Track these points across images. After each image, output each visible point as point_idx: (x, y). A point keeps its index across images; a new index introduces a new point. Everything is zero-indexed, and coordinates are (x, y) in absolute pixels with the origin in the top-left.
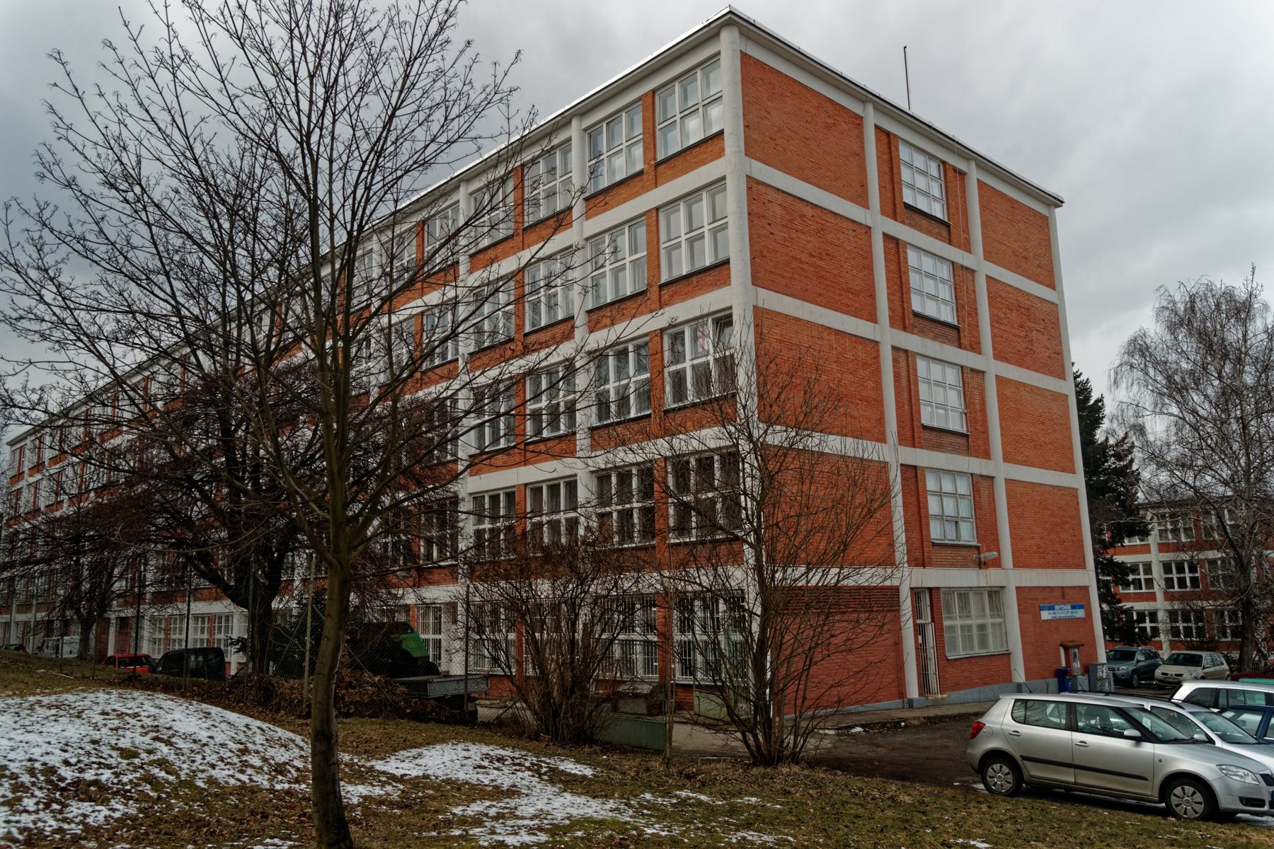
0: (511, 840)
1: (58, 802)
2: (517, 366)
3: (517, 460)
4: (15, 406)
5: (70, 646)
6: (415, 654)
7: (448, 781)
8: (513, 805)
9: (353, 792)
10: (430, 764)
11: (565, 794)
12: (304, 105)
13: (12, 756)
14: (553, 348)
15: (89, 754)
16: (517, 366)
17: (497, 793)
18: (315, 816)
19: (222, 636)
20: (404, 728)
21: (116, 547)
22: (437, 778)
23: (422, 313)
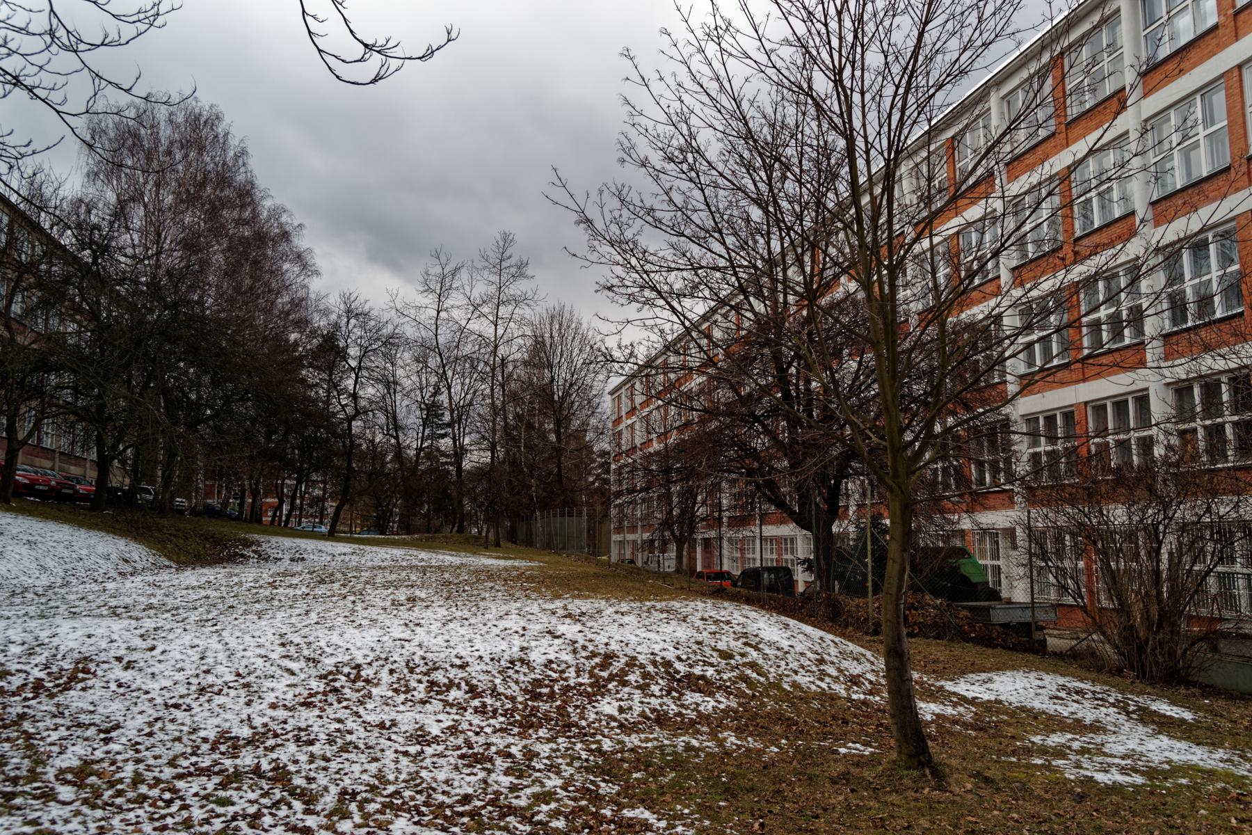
0: (1100, 777)
1: (677, 691)
2: (1079, 271)
3: (1074, 376)
4: (613, 361)
5: (669, 561)
6: (974, 579)
7: (1023, 709)
8: (1099, 740)
9: (928, 709)
10: (1001, 689)
11: (1161, 736)
12: (835, 43)
13: (639, 649)
14: (1119, 247)
15: (695, 652)
16: (1079, 271)
17: (1078, 726)
18: (894, 728)
19: (789, 557)
20: (971, 652)
21: (699, 476)
22: (1010, 704)
23: (958, 233)
